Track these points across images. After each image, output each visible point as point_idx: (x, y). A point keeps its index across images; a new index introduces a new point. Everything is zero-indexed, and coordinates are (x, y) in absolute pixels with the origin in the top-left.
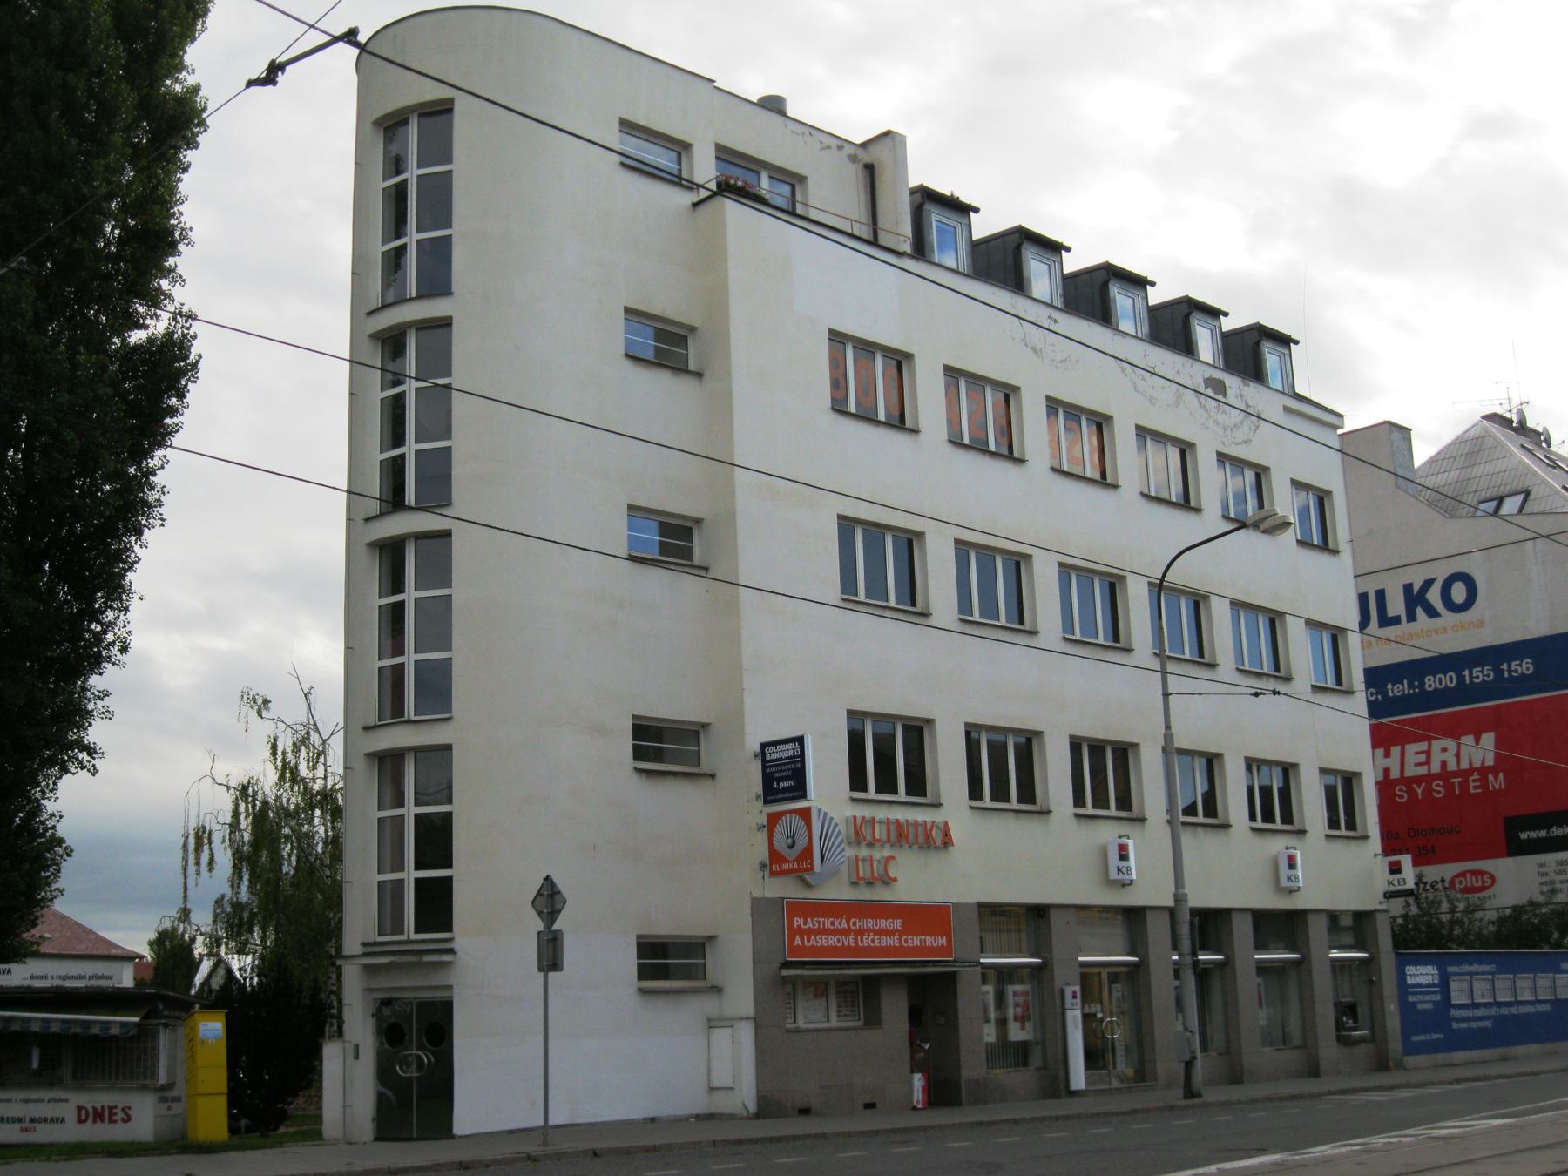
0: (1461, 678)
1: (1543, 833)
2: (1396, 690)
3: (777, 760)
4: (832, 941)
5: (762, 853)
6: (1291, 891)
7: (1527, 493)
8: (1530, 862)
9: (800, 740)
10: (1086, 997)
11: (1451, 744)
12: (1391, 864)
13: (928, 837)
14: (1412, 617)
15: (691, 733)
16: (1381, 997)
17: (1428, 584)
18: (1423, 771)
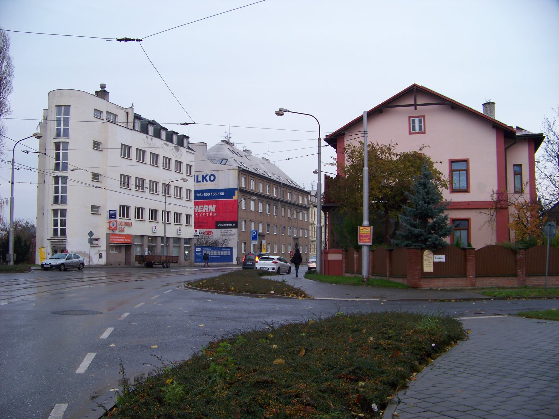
0: (211, 194)
1: (222, 225)
2: (198, 195)
4: (116, 240)
5: (108, 227)
6: (155, 233)
7: (227, 160)
8: (219, 230)
9: (116, 210)
10: (148, 250)
11: (207, 206)
13: (129, 224)
14: (203, 181)
15: (98, 207)
16: (192, 253)
17: (207, 175)
18: (202, 211)
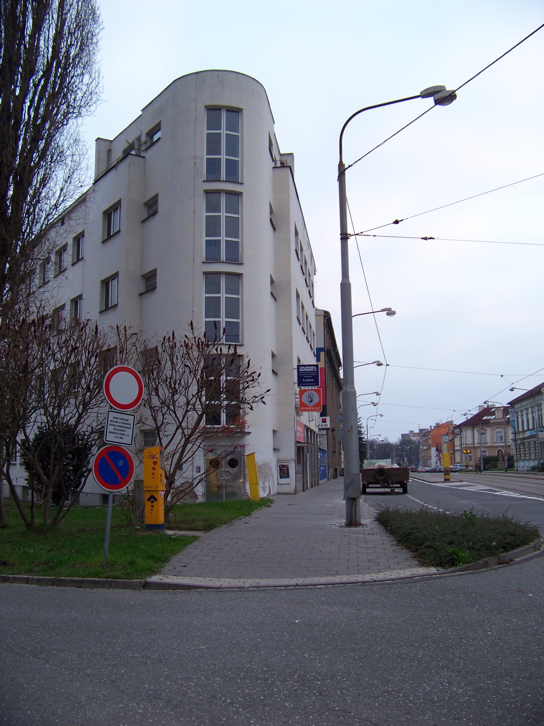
3: (305, 371)
12: (323, 419)
